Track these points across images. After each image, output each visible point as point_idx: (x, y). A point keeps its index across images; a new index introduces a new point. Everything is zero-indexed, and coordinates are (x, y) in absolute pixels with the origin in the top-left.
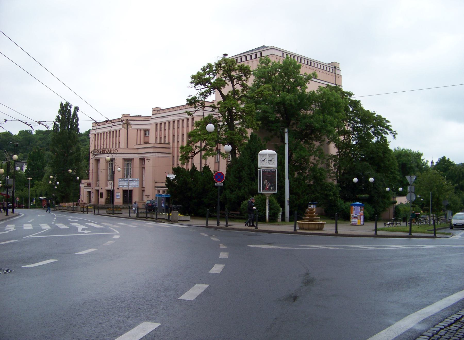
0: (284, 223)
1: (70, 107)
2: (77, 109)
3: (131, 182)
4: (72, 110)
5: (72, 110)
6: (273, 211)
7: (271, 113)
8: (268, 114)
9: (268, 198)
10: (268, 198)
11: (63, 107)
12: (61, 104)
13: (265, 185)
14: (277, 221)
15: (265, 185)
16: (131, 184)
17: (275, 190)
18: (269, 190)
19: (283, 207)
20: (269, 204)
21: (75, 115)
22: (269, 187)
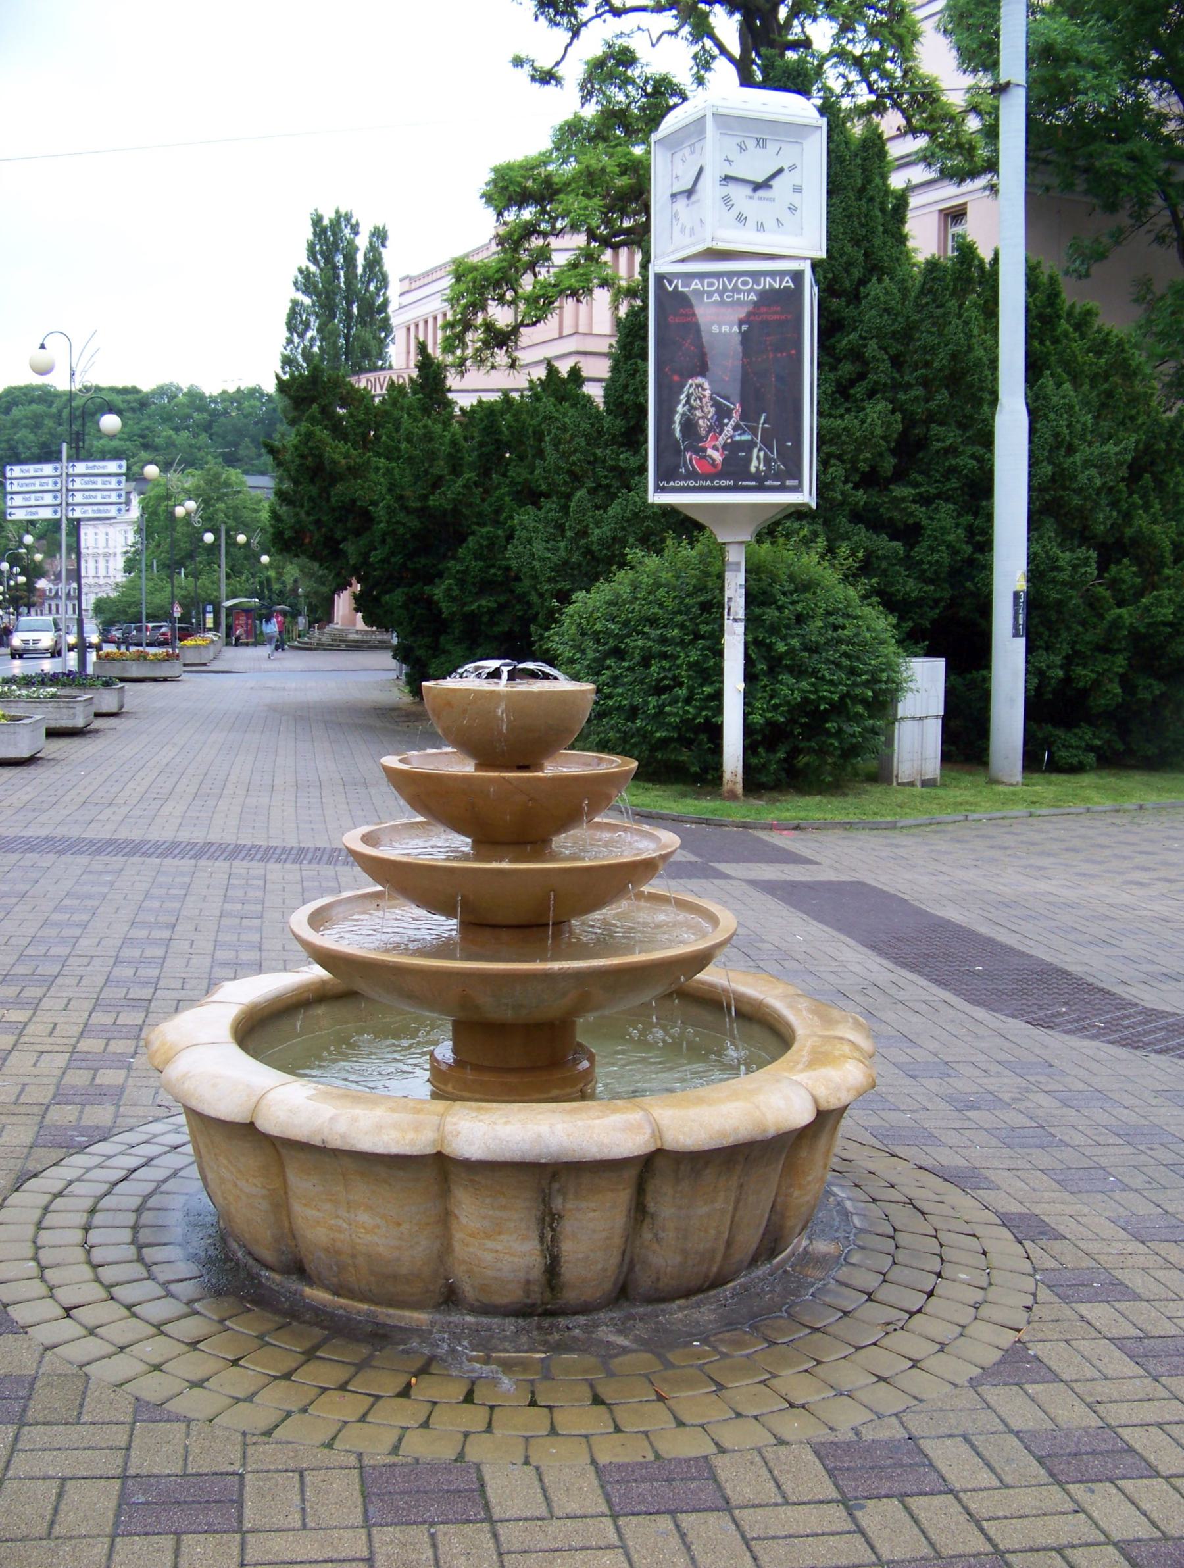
0: (965, 789)
1: (355, 230)
2: (380, 235)
3: (79, 483)
4: (362, 242)
5: (362, 242)
6: (791, 689)
7: (1093, 65)
8: (1072, 70)
9: (736, 556)
10: (736, 556)
11: (324, 230)
12: (317, 221)
13: (689, 425)
14: (882, 775)
15: (689, 425)
16: (79, 498)
17: (788, 475)
18: (734, 472)
19: (968, 658)
20: (751, 621)
21: (374, 262)
22: (732, 448)
